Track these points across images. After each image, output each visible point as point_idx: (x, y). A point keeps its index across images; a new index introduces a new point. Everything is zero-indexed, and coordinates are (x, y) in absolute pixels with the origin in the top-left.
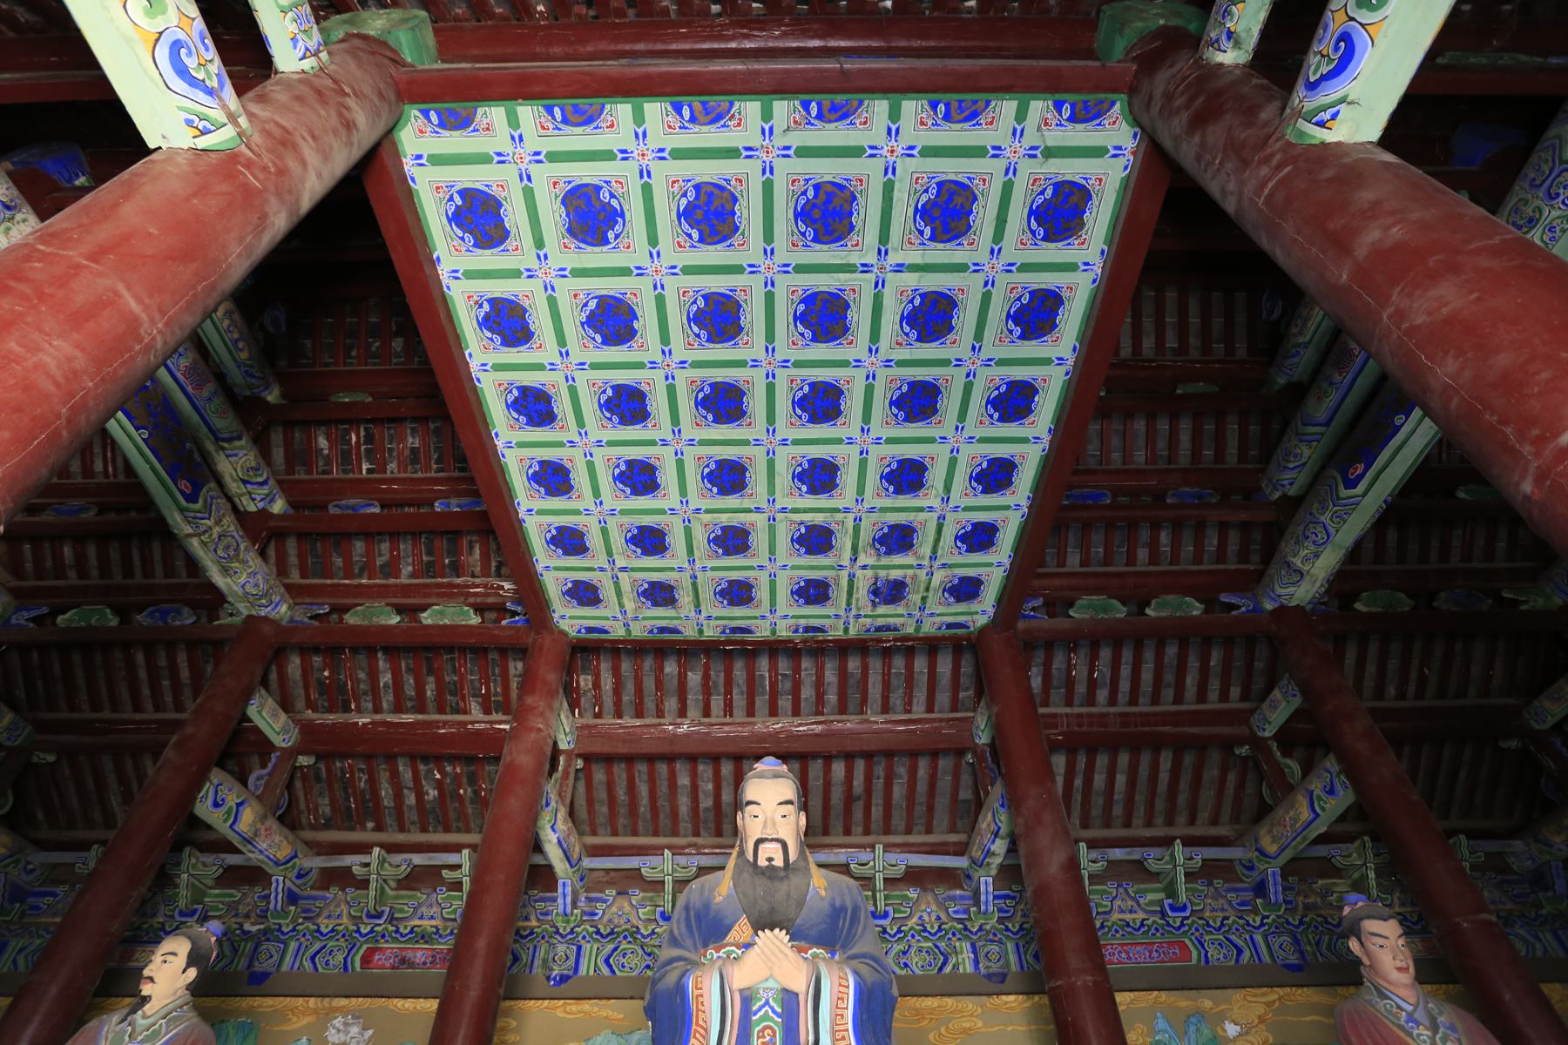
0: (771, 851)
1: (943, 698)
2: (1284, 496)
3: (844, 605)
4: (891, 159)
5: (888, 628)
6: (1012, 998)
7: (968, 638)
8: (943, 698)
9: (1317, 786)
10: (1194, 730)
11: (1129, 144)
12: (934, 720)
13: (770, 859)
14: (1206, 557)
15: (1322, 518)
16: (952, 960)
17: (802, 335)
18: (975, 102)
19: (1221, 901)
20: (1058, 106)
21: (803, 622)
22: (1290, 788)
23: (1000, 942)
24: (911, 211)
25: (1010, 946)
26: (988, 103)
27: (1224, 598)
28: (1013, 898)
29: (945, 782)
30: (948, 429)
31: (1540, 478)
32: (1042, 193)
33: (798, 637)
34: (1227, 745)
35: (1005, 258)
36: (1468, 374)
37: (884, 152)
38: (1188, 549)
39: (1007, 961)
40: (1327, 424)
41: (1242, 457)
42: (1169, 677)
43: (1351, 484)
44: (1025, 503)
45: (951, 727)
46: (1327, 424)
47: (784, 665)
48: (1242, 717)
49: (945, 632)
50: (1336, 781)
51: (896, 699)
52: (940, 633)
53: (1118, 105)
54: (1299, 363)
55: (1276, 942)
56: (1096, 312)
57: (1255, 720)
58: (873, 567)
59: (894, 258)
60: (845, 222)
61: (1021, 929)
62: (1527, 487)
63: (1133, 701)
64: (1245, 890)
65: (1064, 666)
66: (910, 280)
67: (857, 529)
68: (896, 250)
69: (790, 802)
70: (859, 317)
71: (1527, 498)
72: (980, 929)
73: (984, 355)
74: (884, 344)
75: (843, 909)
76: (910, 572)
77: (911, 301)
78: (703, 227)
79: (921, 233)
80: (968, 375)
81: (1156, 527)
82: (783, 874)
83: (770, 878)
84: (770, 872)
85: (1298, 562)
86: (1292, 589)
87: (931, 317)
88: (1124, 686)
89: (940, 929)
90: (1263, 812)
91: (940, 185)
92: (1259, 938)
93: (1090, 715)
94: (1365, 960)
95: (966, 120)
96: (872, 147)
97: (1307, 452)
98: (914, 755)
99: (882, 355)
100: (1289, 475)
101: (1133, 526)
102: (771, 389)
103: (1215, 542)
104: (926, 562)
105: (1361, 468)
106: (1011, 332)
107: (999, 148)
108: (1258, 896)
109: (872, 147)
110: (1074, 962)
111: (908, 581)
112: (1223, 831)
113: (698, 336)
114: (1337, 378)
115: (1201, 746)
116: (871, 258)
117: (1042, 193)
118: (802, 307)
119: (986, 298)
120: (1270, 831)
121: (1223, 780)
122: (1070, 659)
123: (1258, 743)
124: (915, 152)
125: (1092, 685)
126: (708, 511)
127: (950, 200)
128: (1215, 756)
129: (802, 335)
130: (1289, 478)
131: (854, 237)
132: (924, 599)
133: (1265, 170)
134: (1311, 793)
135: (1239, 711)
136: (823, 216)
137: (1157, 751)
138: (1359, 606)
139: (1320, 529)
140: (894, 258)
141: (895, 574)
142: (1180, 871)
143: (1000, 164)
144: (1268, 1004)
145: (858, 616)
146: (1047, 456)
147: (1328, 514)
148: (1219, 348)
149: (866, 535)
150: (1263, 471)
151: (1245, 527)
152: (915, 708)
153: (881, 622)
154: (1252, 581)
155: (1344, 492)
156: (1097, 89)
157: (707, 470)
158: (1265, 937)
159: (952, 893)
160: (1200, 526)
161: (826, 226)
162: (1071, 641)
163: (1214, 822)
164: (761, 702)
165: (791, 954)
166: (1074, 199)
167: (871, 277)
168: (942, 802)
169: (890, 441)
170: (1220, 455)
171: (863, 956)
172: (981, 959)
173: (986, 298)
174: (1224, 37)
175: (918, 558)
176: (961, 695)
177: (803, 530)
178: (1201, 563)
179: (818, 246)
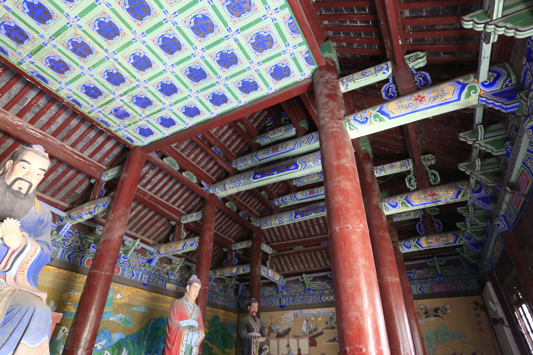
0: (24, 186)
1: (98, 156)
2: (236, 168)
3: (99, 105)
4: (268, 15)
5: (106, 123)
6: (52, 267)
7: (130, 145)
8: (98, 156)
9: (189, 242)
10: (167, 211)
11: (307, 76)
12: (91, 162)
13: (20, 188)
14: (206, 168)
15: (242, 181)
17: (190, 23)
18: (298, 30)
19: (137, 260)
20: (307, 52)
21: (75, 97)
22: (180, 239)
23: (59, 247)
24: (256, 32)
25: (61, 250)
26: (299, 33)
27: (203, 183)
28: (72, 234)
29: (74, 183)
30: (195, 89)
31: (340, 229)
32: (283, 64)
33: (66, 100)
34: (170, 219)
35: (259, 68)
36: (343, 202)
37: (270, 12)
38: (203, 163)
39: (56, 255)
40: (259, 160)
41: (233, 151)
42: (170, 193)
43: (254, 178)
44: (190, 125)
45: (95, 168)
46: (259, 160)
47: (42, 102)
48: (180, 215)
49: (124, 139)
50: (195, 244)
51: (80, 145)
52: (122, 138)
53: (314, 66)
54: (264, 141)
55: (144, 276)
56: (261, 101)
57: (183, 217)
58: (125, 103)
59: (238, 36)
60: (240, 13)
61: (70, 245)
62: (337, 229)
63: (156, 193)
64: (145, 259)
65: (145, 172)
66: (235, 46)
67: (133, 88)
68: (241, 35)
69: (44, 170)
70: (211, 38)
71: (336, 230)
73: (227, 82)
74: (208, 52)
75: (42, 222)
76: (135, 114)
77: (228, 51)
79: (252, 39)
80: (217, 82)
81: (202, 151)
82: (23, 197)
83: (16, 196)
84: (17, 194)
85: (227, 186)
86: (220, 192)
87: (227, 60)
88: (157, 188)
90: (166, 241)
91: (269, 35)
92: (140, 274)
93: (142, 191)
94: (188, 292)
95: (292, 30)
96: (269, 7)
97: (250, 163)
98: (70, 167)
99: (204, 54)
100: (242, 164)
101: (197, 146)
103: (211, 166)
104: (143, 116)
105: (260, 176)
106: (239, 84)
107: (289, 45)
108: (147, 262)
109: (269, 7)
110: (106, 267)
111: (131, 116)
112: (150, 241)
114: (270, 152)
115: (163, 215)
116: (234, 29)
117: (283, 64)
118: (201, 16)
119: (244, 71)
120: (166, 248)
121: (161, 227)
122: (149, 170)
123: (179, 223)
124: (275, 21)
125: (149, 181)
126: (84, 31)
127: (266, 41)
128: (164, 220)
129: (190, 23)
130: (241, 165)
131: (237, 19)
132: (130, 125)
133: (335, 125)
134: (186, 243)
135: (181, 212)
136: (237, 4)
137: (151, 210)
138: (227, 204)
139: (239, 183)
140: (238, 36)
141: (129, 111)
142: (134, 248)
143: (284, 48)
144: (133, 292)
145: (100, 112)
146: (209, 119)
147: (244, 181)
148: (252, 120)
149: (135, 93)
150: (236, 158)
151: (220, 167)
152: (85, 153)
153: (106, 120)
154: (212, 183)
155: (251, 179)
156: (316, 59)
157: (103, 19)
158: (142, 274)
160: (211, 159)
161: (235, 7)
162: (154, 165)
163: (149, 237)
164: (17, 108)
165: (18, 231)
166: (286, 73)
167: (227, 33)
168: (67, 189)
169: (176, 76)
170: (230, 146)
171: (44, 242)
173: (244, 71)
174: (346, 84)
175: (143, 113)
176: (106, 159)
177: (115, 72)
179: (226, 8)
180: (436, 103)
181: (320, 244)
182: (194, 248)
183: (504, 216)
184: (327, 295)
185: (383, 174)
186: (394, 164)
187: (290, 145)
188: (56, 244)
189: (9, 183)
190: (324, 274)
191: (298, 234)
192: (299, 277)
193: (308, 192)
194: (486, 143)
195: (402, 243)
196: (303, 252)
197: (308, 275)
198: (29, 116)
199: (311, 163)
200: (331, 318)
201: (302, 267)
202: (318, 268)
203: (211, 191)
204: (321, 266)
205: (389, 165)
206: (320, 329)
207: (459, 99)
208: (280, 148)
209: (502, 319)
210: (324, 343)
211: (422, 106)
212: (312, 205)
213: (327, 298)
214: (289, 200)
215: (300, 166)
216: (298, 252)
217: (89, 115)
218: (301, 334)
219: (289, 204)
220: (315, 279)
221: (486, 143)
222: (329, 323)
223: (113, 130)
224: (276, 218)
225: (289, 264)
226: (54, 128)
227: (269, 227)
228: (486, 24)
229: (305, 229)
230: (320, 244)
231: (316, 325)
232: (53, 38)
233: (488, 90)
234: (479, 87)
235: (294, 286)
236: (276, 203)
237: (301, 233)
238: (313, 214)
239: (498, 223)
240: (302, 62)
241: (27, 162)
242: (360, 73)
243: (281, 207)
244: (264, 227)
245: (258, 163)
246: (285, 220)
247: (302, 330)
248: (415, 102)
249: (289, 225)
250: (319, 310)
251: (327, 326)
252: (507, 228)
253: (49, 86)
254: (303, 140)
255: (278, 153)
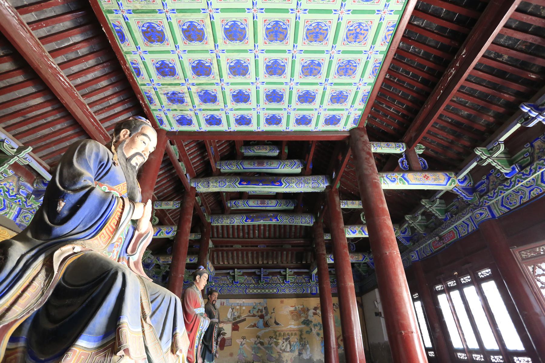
16: (7, 210)
43: (240, 184)
72: (30, 206)
78: (354, 31)
85: (211, 184)
89: (15, 196)
100: (226, 168)
102: (284, 51)
105: (245, 183)
113: (311, 25)
114: (256, 165)
118: (317, 62)
130: (225, 168)
138: (197, 198)
155: (237, 184)
159: (26, 183)
172: (21, 217)
178: (108, 131)
180: (435, 183)
181: (257, 246)
182: (170, 236)
183: (417, 251)
184: (252, 288)
185: (346, 207)
186: (354, 202)
187: (275, 164)
188: (32, 211)
189: (128, 156)
190: (253, 271)
191: (238, 235)
192: (231, 272)
193: (259, 202)
194: (436, 210)
195: (329, 256)
196: (241, 250)
197: (239, 271)
198: (61, 59)
199: (294, 185)
200: (254, 308)
201: (231, 263)
202: (246, 265)
203: (193, 185)
204: (248, 263)
205: (351, 201)
206: (243, 317)
207: (446, 185)
208: (265, 164)
209: (380, 313)
210: (246, 328)
211: (427, 183)
212: (265, 214)
213: (251, 291)
214: (241, 205)
215: (284, 184)
216: (237, 250)
217: (140, 87)
218: (226, 320)
219: (240, 208)
220: (244, 274)
221: (436, 210)
222: (251, 312)
223: (152, 107)
224: (228, 218)
225: (221, 258)
226: (79, 81)
227: (219, 224)
228: (489, 157)
229: (246, 231)
230: (257, 246)
231: (240, 313)
232: (175, 11)
233: (460, 185)
234: (457, 182)
235: (223, 278)
236: (229, 205)
237: (241, 234)
238: (262, 221)
239: (413, 255)
240: (351, 120)
241: (149, 138)
242: (386, 143)
243: (232, 208)
244: (214, 224)
245: (243, 170)
246: (236, 221)
247: (227, 317)
248: (424, 179)
249: (238, 226)
250: (244, 300)
251: (249, 314)
252: (417, 259)
253: (122, 45)
254: (286, 163)
255: (262, 167)
